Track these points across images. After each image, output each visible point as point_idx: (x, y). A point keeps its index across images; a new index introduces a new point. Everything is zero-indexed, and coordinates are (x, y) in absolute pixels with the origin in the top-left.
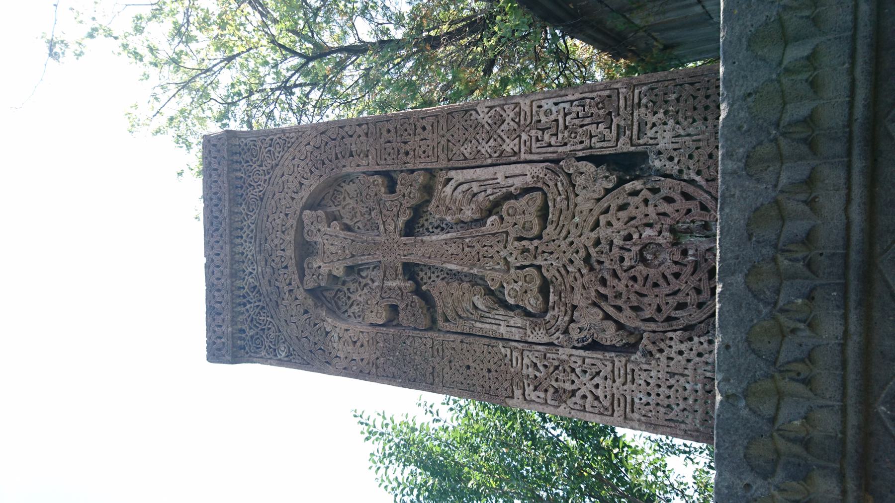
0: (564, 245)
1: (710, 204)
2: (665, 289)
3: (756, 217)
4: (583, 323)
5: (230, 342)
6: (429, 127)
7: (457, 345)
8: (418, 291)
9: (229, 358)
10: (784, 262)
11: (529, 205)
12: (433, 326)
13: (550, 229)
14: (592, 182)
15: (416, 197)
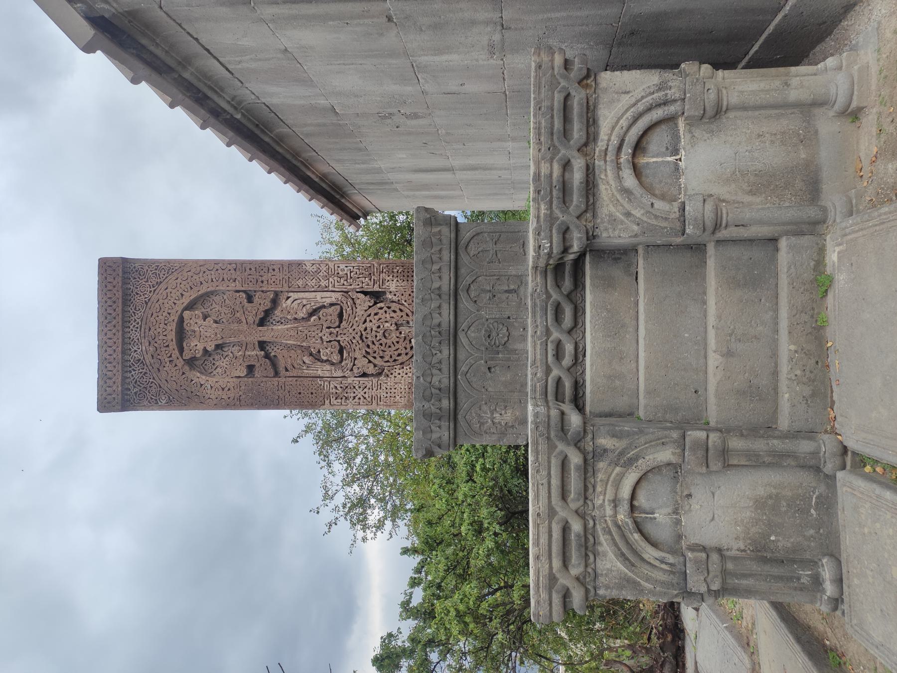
0: (351, 331)
1: (410, 314)
2: (393, 348)
7: (294, 383)
8: (267, 356)
10: (433, 332)
11: (335, 310)
13: (344, 323)
14: (364, 302)
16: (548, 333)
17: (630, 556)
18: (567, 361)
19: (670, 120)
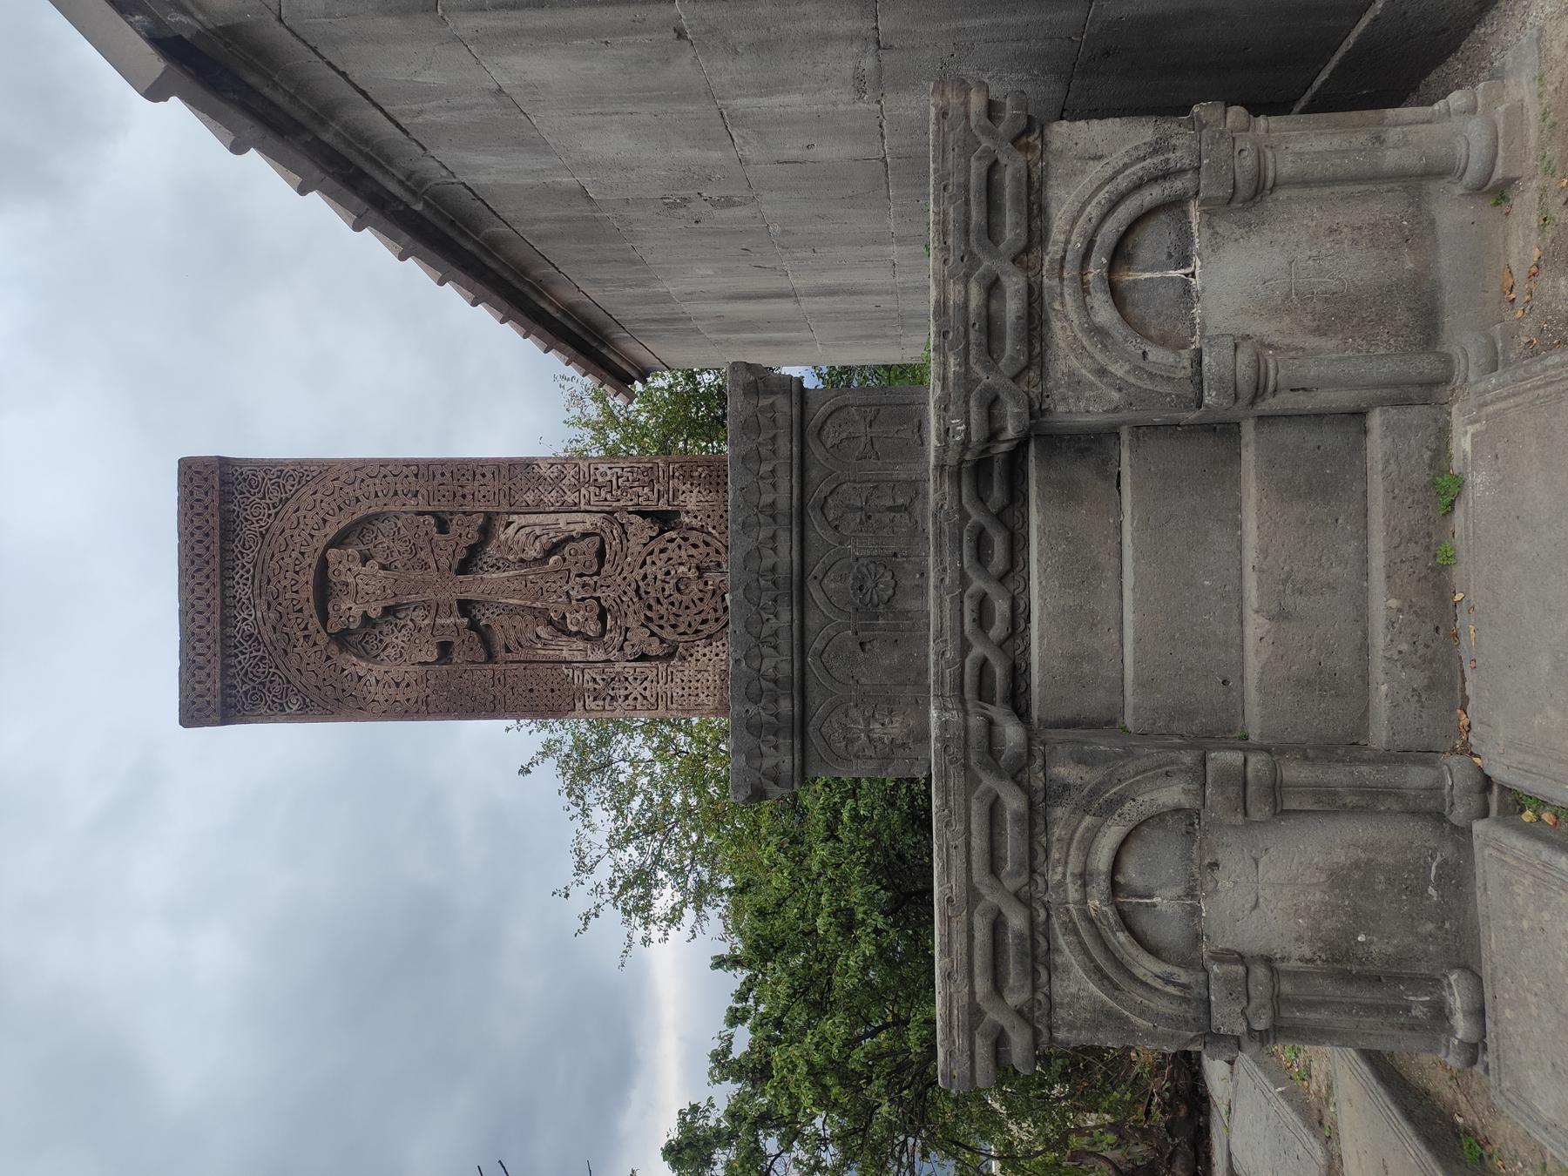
0: (619, 580)
1: (722, 550)
3: (748, 557)
4: (635, 640)
5: (219, 699)
6: (489, 475)
7: (520, 672)
8: (474, 625)
9: (218, 718)
10: (762, 582)
11: (590, 545)
12: (491, 657)
13: (607, 566)
14: (640, 530)
15: (474, 537)
16: (964, 581)
17: (1111, 972)
18: (998, 630)
19: (1175, 205)
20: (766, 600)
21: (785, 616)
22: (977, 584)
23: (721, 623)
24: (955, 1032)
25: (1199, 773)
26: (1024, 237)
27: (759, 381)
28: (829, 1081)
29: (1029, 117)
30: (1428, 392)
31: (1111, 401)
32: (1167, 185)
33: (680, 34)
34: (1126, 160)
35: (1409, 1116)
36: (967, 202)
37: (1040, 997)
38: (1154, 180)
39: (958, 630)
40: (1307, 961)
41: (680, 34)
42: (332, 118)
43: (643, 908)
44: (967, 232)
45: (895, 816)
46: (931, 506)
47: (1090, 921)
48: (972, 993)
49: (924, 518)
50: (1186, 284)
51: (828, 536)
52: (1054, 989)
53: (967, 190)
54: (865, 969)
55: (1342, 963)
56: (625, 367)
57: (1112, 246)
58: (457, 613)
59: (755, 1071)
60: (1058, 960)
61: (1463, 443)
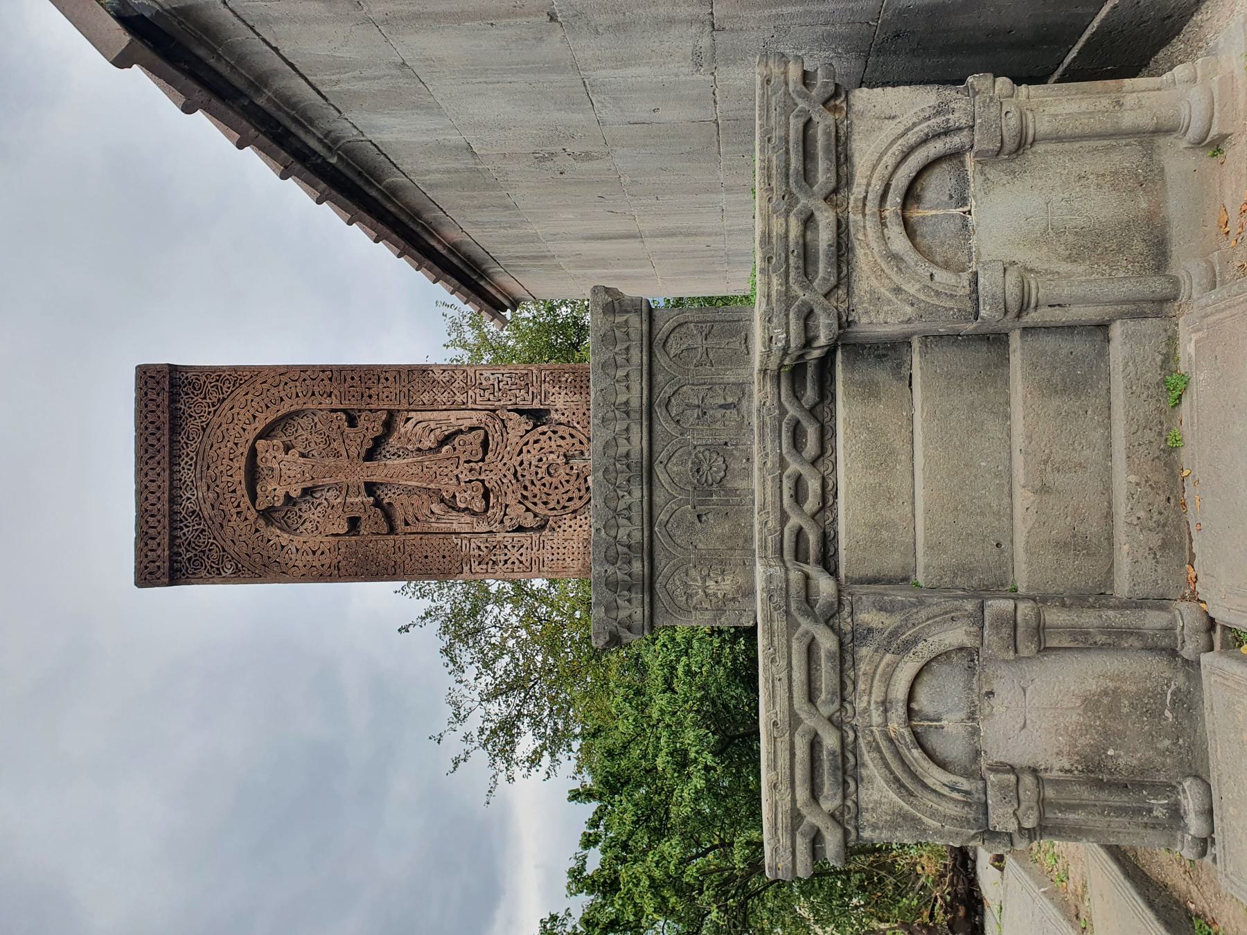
0: (500, 466)
1: (585, 441)
3: (606, 446)
4: (513, 515)
5: (167, 564)
9: (167, 580)
10: (618, 466)
13: (490, 454)
14: (518, 425)
15: (378, 430)
16: (783, 464)
17: (908, 782)
18: (811, 504)
19: (955, 156)
20: (621, 480)
21: (637, 494)
22: (794, 467)
23: (584, 501)
24: (780, 832)
25: (978, 619)
26: (834, 180)
27: (613, 304)
28: (666, 893)
29: (837, 85)
30: (1160, 306)
31: (905, 314)
32: (948, 140)
33: (553, 18)
34: (915, 120)
35: (1151, 904)
36: (787, 152)
37: (849, 803)
38: (937, 136)
39: (778, 504)
40: (1067, 771)
41: (553, 18)
42: (266, 86)
43: (506, 753)
44: (787, 176)
45: (721, 672)
46: (756, 403)
47: (891, 740)
48: (794, 800)
49: (750, 414)
50: (965, 219)
51: (670, 427)
52: (861, 797)
53: (787, 142)
54: (696, 800)
55: (1094, 773)
56: (499, 297)
57: (905, 189)
58: (364, 493)
59: (606, 885)
60: (864, 772)
61: (1188, 348)
